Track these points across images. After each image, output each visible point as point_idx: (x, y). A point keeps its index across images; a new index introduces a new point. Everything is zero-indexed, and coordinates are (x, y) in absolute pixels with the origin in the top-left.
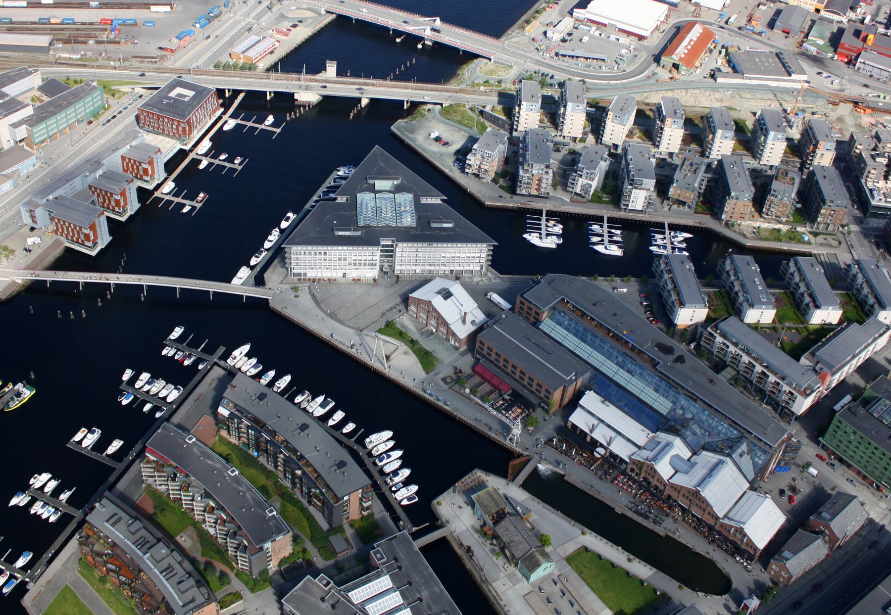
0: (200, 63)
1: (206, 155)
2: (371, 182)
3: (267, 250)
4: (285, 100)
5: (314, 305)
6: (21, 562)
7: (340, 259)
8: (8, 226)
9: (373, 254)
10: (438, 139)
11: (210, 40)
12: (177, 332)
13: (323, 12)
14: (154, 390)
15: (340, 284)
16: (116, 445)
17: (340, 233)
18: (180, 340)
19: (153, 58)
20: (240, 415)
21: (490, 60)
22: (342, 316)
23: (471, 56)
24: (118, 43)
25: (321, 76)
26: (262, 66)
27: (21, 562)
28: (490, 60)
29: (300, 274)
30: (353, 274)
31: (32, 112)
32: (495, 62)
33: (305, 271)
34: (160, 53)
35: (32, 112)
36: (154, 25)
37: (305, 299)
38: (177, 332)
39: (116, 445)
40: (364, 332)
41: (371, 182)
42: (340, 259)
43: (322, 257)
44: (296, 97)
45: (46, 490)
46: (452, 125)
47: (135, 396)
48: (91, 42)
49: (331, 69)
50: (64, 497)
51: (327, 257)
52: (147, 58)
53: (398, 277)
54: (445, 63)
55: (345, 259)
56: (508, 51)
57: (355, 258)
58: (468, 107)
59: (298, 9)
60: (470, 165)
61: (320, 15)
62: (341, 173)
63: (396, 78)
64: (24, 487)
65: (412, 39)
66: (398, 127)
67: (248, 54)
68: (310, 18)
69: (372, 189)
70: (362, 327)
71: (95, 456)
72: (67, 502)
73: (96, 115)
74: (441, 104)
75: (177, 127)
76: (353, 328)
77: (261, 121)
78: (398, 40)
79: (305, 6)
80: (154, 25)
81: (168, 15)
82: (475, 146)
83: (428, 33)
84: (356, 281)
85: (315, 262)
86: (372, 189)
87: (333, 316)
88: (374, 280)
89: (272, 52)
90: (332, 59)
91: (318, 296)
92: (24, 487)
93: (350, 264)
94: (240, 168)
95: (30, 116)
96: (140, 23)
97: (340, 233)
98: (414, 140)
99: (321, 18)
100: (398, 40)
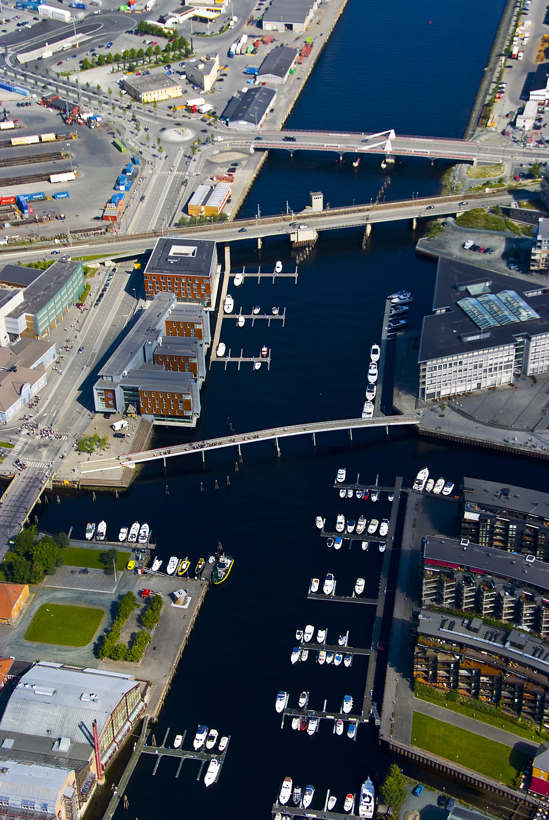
0: (152, 226)
1: (236, 311)
2: (462, 288)
3: (376, 383)
4: (280, 246)
5: (466, 420)
6: (347, 707)
7: (475, 367)
8: (74, 420)
9: (505, 354)
10: (474, 248)
11: (146, 201)
12: (342, 475)
13: (252, 151)
14: (361, 528)
15: (478, 396)
16: (360, 586)
17: (470, 339)
18: (349, 480)
19: (97, 229)
20: (492, 514)
21: (471, 163)
22: (503, 422)
23: (448, 164)
24: (41, 221)
25: (307, 211)
26: (231, 211)
27: (347, 707)
28: (471, 163)
29: (433, 395)
30: (487, 383)
31: (22, 300)
32: (479, 164)
33: (438, 390)
34: (99, 223)
35: (22, 300)
36: (68, 196)
37: (453, 417)
38: (342, 475)
39: (360, 586)
40: (536, 432)
41: (462, 288)
42: (475, 367)
43: (459, 367)
44: (293, 238)
45: (320, 640)
46: (479, 233)
47: (343, 539)
48: (7, 225)
49: (318, 202)
50: (343, 641)
51: (463, 367)
52: (90, 230)
53: (533, 377)
54: (426, 177)
55: (481, 366)
56: (487, 150)
57: (490, 362)
58: (486, 211)
59: (221, 152)
60: (534, 260)
61: (250, 154)
62: (396, 300)
63: (381, 201)
64: (296, 645)
65: (372, 160)
66: (423, 245)
67: (210, 204)
68: (243, 160)
69: (467, 294)
70: (532, 428)
71: (343, 599)
72: (349, 644)
73: (82, 296)
74: (454, 215)
75: (199, 286)
76: (523, 430)
77: (272, 270)
78: (356, 164)
79: (228, 148)
80: (68, 196)
81: (73, 183)
82: (539, 238)
83: (389, 149)
84: (493, 389)
85: (448, 377)
86: (467, 294)
87: (493, 424)
88: (510, 384)
89: (229, 201)
90: (315, 190)
91: (465, 410)
92: (296, 645)
93: (485, 371)
94: (283, 317)
95: (22, 304)
96: (49, 196)
97: (470, 339)
98: (450, 254)
99: (255, 158)
100: (356, 164)
